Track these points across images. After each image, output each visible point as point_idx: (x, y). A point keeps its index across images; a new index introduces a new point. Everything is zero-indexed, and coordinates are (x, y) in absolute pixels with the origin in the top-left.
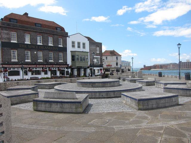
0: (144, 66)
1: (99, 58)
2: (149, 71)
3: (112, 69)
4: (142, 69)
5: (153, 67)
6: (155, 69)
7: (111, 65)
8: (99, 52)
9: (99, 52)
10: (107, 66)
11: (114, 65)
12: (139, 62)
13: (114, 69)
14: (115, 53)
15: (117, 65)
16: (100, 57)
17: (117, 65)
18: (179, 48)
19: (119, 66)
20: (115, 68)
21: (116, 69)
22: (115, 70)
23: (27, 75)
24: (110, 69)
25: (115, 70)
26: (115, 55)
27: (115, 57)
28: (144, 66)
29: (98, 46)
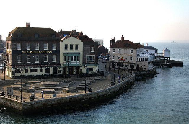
9: (94, 52)
21: (129, 65)
24: (123, 64)
29: (93, 46)
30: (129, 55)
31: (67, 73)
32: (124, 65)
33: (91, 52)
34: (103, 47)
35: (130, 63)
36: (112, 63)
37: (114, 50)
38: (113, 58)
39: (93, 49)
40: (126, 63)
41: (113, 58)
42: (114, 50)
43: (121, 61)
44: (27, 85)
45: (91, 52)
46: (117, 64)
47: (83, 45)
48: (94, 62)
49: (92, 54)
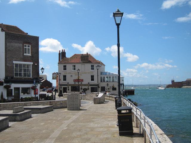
0: (173, 81)
1: (30, 65)
2: (179, 89)
3: (83, 87)
4: (168, 86)
5: (185, 83)
6: (189, 87)
7: (82, 80)
8: (30, 55)
9: (30, 55)
10: (75, 81)
11: (87, 80)
12: (146, 77)
13: (86, 87)
14: (89, 59)
15: (92, 79)
16: (32, 63)
17: (92, 79)
18: (98, 69)
19: (95, 82)
20: (89, 84)
21: (90, 87)
22: (88, 89)
23: (94, 76)
24: (80, 87)
25: (88, 89)
26: (90, 62)
27: (89, 66)
28: (173, 81)
29: (29, 43)
30: (88, 73)
31: (128, 120)
32: (81, 89)
33: (25, 54)
34: (46, 81)
35: (91, 85)
36: (63, 87)
37: (65, 67)
38: (65, 79)
39: (29, 49)
40: (85, 85)
41: (65, 79)
42: (65, 67)
43: (77, 83)
44: (54, 110)
45: (25, 54)
46: (70, 87)
47: (6, 39)
48: (31, 77)
49: (25, 59)
